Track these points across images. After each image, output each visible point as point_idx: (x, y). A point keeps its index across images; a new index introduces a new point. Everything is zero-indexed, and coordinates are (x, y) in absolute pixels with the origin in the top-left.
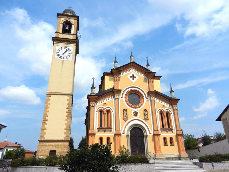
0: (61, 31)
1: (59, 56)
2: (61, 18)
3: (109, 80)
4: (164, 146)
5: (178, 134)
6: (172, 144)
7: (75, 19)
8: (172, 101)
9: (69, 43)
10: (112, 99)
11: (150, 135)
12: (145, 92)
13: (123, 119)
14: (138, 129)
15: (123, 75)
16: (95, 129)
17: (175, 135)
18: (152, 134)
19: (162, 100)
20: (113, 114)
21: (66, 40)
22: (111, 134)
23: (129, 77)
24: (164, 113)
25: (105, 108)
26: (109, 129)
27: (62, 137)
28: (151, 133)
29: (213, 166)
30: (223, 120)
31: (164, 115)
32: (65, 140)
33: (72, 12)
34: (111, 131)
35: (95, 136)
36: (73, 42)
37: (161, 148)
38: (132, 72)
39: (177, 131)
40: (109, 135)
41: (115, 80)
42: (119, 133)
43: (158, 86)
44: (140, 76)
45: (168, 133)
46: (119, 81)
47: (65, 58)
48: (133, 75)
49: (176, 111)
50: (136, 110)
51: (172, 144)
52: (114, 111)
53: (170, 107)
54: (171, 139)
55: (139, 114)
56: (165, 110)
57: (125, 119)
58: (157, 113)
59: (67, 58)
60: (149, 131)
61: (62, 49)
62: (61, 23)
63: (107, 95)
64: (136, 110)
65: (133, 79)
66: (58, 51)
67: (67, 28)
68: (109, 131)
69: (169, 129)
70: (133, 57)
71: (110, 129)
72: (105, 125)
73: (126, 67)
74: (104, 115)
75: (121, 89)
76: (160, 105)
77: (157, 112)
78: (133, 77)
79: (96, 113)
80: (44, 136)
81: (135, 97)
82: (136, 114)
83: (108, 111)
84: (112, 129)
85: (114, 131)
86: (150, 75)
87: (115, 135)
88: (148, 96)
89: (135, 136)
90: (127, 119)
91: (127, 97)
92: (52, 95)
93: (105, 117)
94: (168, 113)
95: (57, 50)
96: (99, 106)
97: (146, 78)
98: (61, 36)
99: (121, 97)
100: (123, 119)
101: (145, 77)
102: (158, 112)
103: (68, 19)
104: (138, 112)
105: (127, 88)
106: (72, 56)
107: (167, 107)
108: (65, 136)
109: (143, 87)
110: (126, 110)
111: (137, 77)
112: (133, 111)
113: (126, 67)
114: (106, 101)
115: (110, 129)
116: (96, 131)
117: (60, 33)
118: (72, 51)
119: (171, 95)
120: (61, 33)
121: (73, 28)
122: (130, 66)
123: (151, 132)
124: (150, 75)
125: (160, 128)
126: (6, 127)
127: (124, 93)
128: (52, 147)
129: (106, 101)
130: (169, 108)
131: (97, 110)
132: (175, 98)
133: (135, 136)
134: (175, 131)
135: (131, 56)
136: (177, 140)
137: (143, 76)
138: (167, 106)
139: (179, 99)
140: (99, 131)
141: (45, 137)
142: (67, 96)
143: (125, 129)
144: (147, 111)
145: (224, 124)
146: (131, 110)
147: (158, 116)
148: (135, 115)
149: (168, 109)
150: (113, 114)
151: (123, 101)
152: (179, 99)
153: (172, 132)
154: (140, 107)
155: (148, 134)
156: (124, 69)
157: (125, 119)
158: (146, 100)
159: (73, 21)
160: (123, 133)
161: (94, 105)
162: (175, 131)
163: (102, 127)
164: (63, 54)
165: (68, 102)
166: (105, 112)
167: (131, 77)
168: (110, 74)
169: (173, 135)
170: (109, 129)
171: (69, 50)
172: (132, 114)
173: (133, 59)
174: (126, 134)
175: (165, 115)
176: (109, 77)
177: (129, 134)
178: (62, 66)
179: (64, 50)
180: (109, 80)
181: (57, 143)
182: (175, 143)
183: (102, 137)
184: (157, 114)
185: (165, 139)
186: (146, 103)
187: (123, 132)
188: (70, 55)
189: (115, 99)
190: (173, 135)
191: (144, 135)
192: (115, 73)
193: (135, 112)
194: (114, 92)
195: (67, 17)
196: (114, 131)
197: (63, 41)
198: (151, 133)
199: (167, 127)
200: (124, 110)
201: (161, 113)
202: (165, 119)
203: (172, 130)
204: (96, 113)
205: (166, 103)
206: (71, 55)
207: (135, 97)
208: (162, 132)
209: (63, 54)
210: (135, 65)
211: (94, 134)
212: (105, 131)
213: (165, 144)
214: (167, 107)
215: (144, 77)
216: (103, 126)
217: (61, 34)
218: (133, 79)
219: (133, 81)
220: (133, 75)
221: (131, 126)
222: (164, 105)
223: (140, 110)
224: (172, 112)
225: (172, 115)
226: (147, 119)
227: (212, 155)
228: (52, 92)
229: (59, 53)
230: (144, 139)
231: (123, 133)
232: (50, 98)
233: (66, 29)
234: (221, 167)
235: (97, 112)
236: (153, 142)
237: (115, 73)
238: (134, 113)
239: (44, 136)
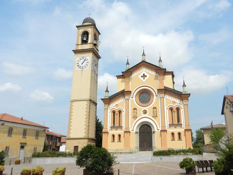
0: (80, 42)
1: (79, 67)
2: (80, 29)
3: (155, 80)
4: (178, 140)
8: (183, 96)
9: (86, 52)
10: (123, 100)
11: (159, 131)
12: (155, 90)
13: (133, 118)
14: (147, 126)
15: (134, 75)
16: (166, 126)
19: (172, 96)
20: (123, 114)
22: (121, 132)
23: (140, 76)
24: (174, 109)
25: (117, 109)
27: (83, 135)
28: (159, 130)
29: (161, 159)
32: (85, 138)
34: (122, 129)
35: (166, 132)
36: (87, 52)
38: (144, 71)
40: (179, 131)
41: (126, 82)
42: (165, 129)
43: (167, 81)
44: (150, 74)
45: (171, 128)
46: (130, 82)
47: (83, 68)
48: (144, 74)
50: (145, 108)
52: (125, 111)
53: (181, 103)
54: (179, 134)
55: (148, 112)
56: (174, 106)
57: (135, 117)
58: (110, 112)
60: (156, 127)
64: (145, 108)
65: (144, 79)
66: (78, 62)
67: (85, 38)
71: (120, 127)
72: (117, 124)
73: (137, 67)
74: (174, 112)
76: (170, 101)
78: (144, 76)
79: (166, 111)
80: (70, 135)
81: (145, 95)
83: (120, 112)
84: (183, 125)
85: (184, 126)
86: (161, 71)
87: (186, 130)
88: (158, 94)
90: (137, 117)
92: (74, 102)
93: (117, 117)
94: (178, 109)
95: (77, 61)
96: (112, 107)
97: (157, 75)
98: (81, 47)
99: (132, 98)
100: (133, 118)
101: (156, 75)
104: (147, 110)
105: (153, 88)
107: (178, 103)
108: (85, 134)
111: (148, 76)
112: (143, 110)
113: (137, 67)
114: (118, 102)
115: (120, 127)
116: (109, 129)
117: (79, 45)
118: (89, 60)
119: (183, 90)
121: (91, 37)
123: (159, 128)
126: (49, 128)
127: (134, 93)
128: (75, 143)
129: (118, 102)
130: (180, 104)
131: (167, 108)
132: (186, 93)
133: (144, 133)
135: (144, 54)
136: (185, 135)
137: (153, 73)
138: (177, 101)
140: (111, 129)
141: (70, 136)
142: (86, 101)
143: (134, 127)
147: (167, 112)
148: (144, 113)
149: (178, 104)
151: (133, 100)
153: (181, 127)
154: (148, 106)
155: (156, 130)
156: (133, 70)
157: (135, 117)
158: (156, 97)
159: (90, 30)
160: (132, 130)
161: (107, 107)
164: (82, 64)
165: (86, 106)
167: (142, 76)
169: (181, 130)
171: (87, 59)
172: (142, 112)
174: (135, 131)
177: (138, 131)
178: (81, 75)
180: (155, 80)
183: (181, 132)
185: (113, 136)
186: (155, 100)
187: (132, 129)
190: (181, 130)
193: (144, 110)
195: (84, 28)
196: (184, 126)
197: (90, 52)
198: (159, 130)
199: (176, 123)
200: (134, 109)
202: (175, 115)
203: (181, 125)
204: (166, 111)
205: (177, 98)
206: (89, 64)
207: (145, 95)
209: (82, 64)
212: (175, 127)
213: (119, 140)
214: (176, 102)
215: (155, 74)
216: (116, 125)
217: (80, 45)
218: (144, 79)
219: (144, 80)
220: (144, 74)
221: (139, 124)
222: (175, 101)
224: (183, 108)
225: (182, 111)
226: (155, 116)
227: (166, 151)
231: (132, 130)
232: (73, 104)
234: (169, 160)
235: (167, 110)
238: (143, 111)
239: (70, 135)
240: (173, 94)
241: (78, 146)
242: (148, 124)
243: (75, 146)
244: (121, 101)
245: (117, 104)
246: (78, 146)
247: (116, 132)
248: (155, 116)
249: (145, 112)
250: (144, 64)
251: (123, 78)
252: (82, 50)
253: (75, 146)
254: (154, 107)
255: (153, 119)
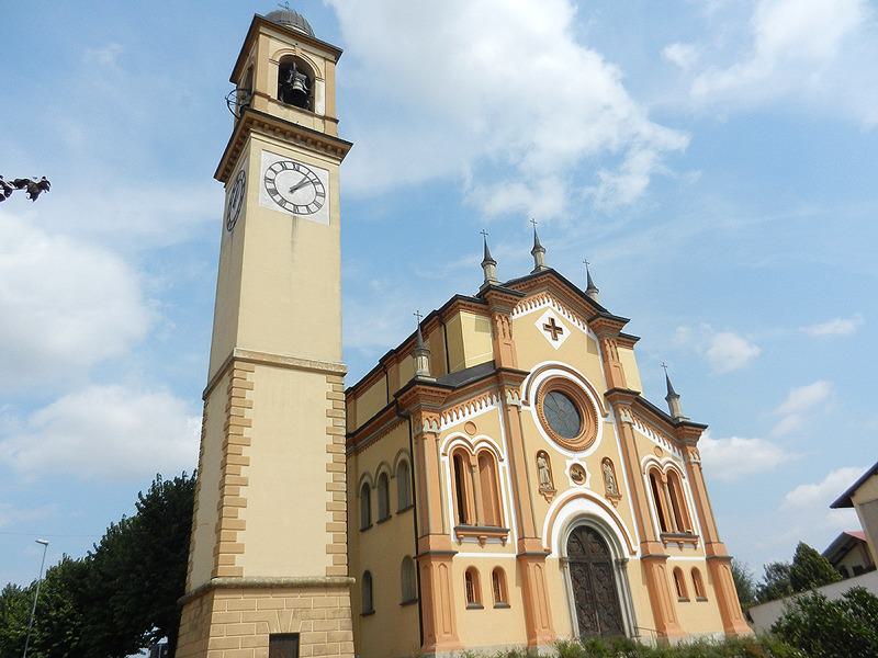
1: (278, 198)
5: (527, 550)
6: (501, 601)
7: (325, 59)
14: (591, 535)
17: (514, 556)
18: (639, 555)
20: (503, 467)
21: (332, 142)
25: (477, 442)
26: (496, 531)
30: (862, 505)
31: (470, 467)
32: (337, 580)
33: (305, 25)
37: (458, 616)
39: (521, 538)
40: (694, 561)
43: (633, 371)
44: (574, 329)
45: (485, 546)
49: (695, 466)
51: (501, 601)
52: (505, 456)
54: (498, 574)
57: (548, 491)
58: (444, 455)
59: (310, 212)
60: (628, 545)
61: (285, 168)
62: (273, 61)
63: (475, 389)
64: (576, 458)
65: (555, 338)
68: (692, 546)
69: (685, 538)
70: (544, 252)
72: (476, 517)
75: (521, 368)
77: (442, 451)
78: (553, 328)
82: (578, 474)
83: (486, 457)
86: (606, 328)
89: (581, 564)
90: (553, 492)
91: (542, 399)
92: (258, 368)
93: (472, 480)
94: (672, 475)
97: (592, 336)
102: (446, 449)
103: (298, 52)
104: (584, 465)
106: (325, 203)
109: (591, 374)
110: (546, 456)
112: (569, 463)
114: (474, 414)
120: (273, 101)
121: (268, 80)
122: (542, 285)
124: (606, 328)
125: (453, 526)
134: (512, 538)
135: (537, 249)
137: (582, 329)
139: (706, 427)
143: (553, 534)
144: (611, 464)
145: (866, 519)
146: (563, 459)
148: (575, 478)
150: (504, 468)
152: (706, 427)
153: (504, 542)
155: (627, 555)
158: (603, 419)
162: (512, 538)
163: (469, 522)
166: (474, 461)
168: (474, 304)
170: (496, 531)
173: (548, 262)
174: (555, 555)
175: (663, 482)
176: (474, 316)
178: (292, 242)
179: (296, 178)
181: (298, 598)
182: (514, 592)
183: (477, 567)
184: (442, 458)
185: (471, 575)
186: (604, 434)
188: (319, 199)
189: (505, 407)
191: (613, 558)
192: (493, 301)
193: (576, 467)
194: (498, 378)
195: (293, 42)
198: (634, 553)
201: (654, 475)
208: (460, 543)
210: (554, 281)
211: (450, 555)
216: (471, 521)
218: (555, 338)
222: (659, 444)
223: (587, 458)
225: (685, 482)
226: (614, 496)
228: (276, 356)
229: (273, 181)
230: (616, 573)
233: (296, 90)
236: (520, 589)
237: (493, 301)
240: (654, 419)
241: (296, 637)
242: (599, 530)
243: (273, 637)
244: (485, 410)
245: (468, 418)
246: (296, 637)
247: (484, 557)
248: (614, 496)
249: (578, 474)
250: (546, 281)
251: (482, 314)
252: (295, 130)
253: (273, 637)
254: (543, 451)
255: (607, 503)
